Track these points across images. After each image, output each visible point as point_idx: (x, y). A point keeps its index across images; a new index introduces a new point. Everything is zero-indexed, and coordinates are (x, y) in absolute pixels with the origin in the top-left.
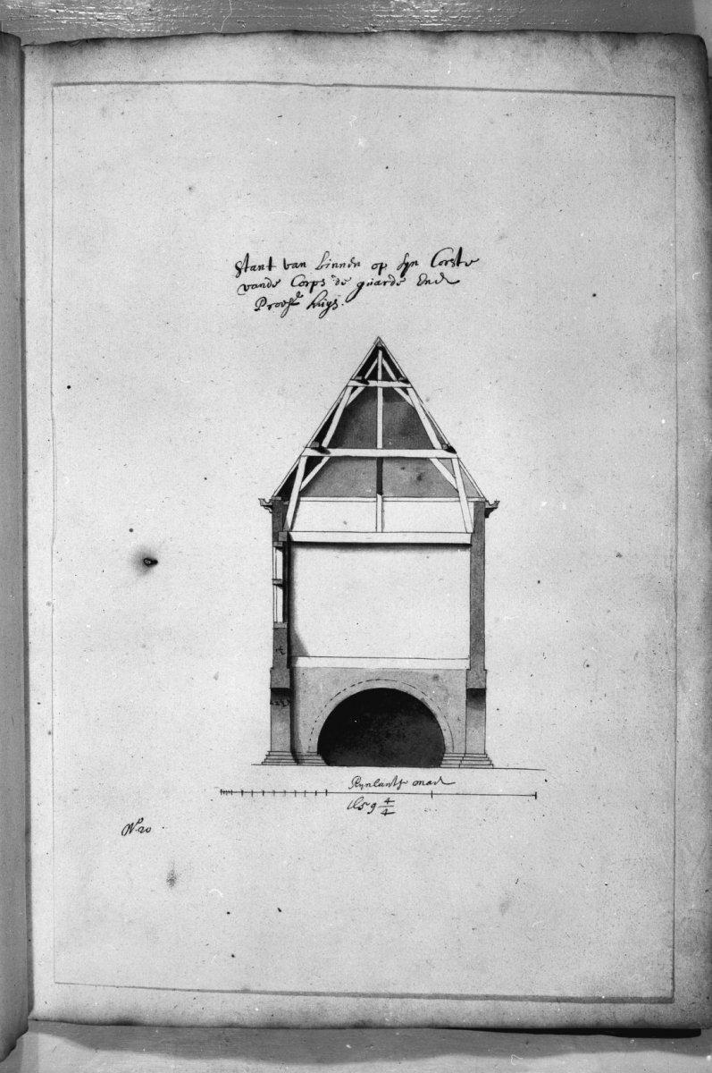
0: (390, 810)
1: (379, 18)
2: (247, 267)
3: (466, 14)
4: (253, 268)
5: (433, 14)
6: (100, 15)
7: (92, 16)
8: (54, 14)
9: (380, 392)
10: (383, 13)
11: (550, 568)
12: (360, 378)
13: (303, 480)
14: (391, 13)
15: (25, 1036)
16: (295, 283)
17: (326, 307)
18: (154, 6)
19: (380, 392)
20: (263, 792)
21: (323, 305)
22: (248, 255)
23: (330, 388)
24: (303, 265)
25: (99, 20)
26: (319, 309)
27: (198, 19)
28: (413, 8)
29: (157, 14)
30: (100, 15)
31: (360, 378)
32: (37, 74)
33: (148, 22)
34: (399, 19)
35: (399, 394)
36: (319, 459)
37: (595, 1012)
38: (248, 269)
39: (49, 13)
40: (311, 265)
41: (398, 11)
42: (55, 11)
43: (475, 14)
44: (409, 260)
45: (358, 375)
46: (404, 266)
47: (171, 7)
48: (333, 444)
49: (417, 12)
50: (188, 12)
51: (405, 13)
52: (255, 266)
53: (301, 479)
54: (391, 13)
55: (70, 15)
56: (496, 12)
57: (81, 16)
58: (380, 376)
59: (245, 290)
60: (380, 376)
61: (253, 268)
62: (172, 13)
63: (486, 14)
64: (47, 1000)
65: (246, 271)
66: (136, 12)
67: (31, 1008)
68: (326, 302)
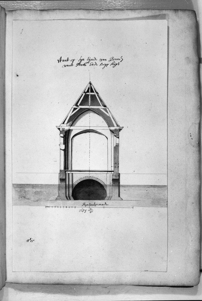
1: (104, 6)
2: (61, 60)
3: (128, 5)
4: (63, 61)
5: (119, 5)
6: (26, 5)
7: (24, 6)
8: (13, 5)
9: (90, 95)
10: (105, 4)
11: (148, 145)
13: (72, 112)
14: (107, 4)
17: (115, 65)
18: (41, 3)
19: (90, 95)
22: (61, 57)
23: (77, 93)
24: (106, 60)
25: (26, 7)
26: (113, 65)
27: (54, 6)
28: (113, 3)
29: (42, 5)
30: (26, 5)
32: (9, 18)
34: (110, 6)
36: (76, 108)
38: (62, 61)
39: (12, 5)
40: (108, 60)
42: (13, 4)
43: (131, 5)
44: (82, 59)
46: (80, 60)
47: (46, 3)
48: (80, 105)
50: (51, 4)
51: (111, 4)
52: (104, 59)
53: (72, 112)
54: (107, 4)
55: (18, 6)
56: (136, 4)
58: (90, 91)
59: (65, 67)
60: (90, 91)
61: (63, 61)
62: (46, 5)
63: (134, 4)
64: (10, 277)
65: (60, 62)
66: (36, 5)
68: (105, 64)
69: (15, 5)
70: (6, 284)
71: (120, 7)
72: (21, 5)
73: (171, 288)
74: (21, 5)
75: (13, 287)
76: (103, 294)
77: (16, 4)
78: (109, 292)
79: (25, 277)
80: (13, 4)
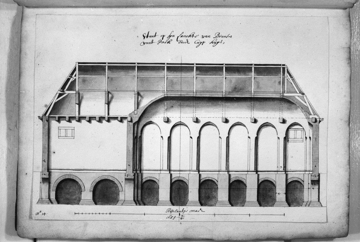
0: (182, 218)
4: (150, 37)
5: (356, 144)
6: (356, 33)
7: (355, 30)
12: (62, 90)
14: (356, 131)
15: (17, 4)
16: (196, 42)
17: (200, 43)
20: (145, 214)
21: (199, 43)
25: (354, 33)
28: (358, 138)
30: (356, 33)
31: (62, 90)
33: (353, 49)
35: (58, 101)
37: (6, 64)
38: (148, 37)
39: (356, 16)
41: (357, 133)
42: (357, 18)
43: (356, 158)
45: (61, 89)
49: (357, 139)
50: (357, 63)
52: (207, 36)
54: (356, 131)
57: (355, 27)
59: (144, 44)
61: (150, 37)
62: (356, 57)
66: (357, 46)
67: (27, 7)
69: (356, 20)
70: (21, 7)
71: (353, 146)
72: (356, 27)
73: (15, 204)
74: (356, 27)
75: (17, 15)
76: (7, 122)
77: (357, 21)
78: (11, 130)
79: (29, 26)
80: (357, 18)
